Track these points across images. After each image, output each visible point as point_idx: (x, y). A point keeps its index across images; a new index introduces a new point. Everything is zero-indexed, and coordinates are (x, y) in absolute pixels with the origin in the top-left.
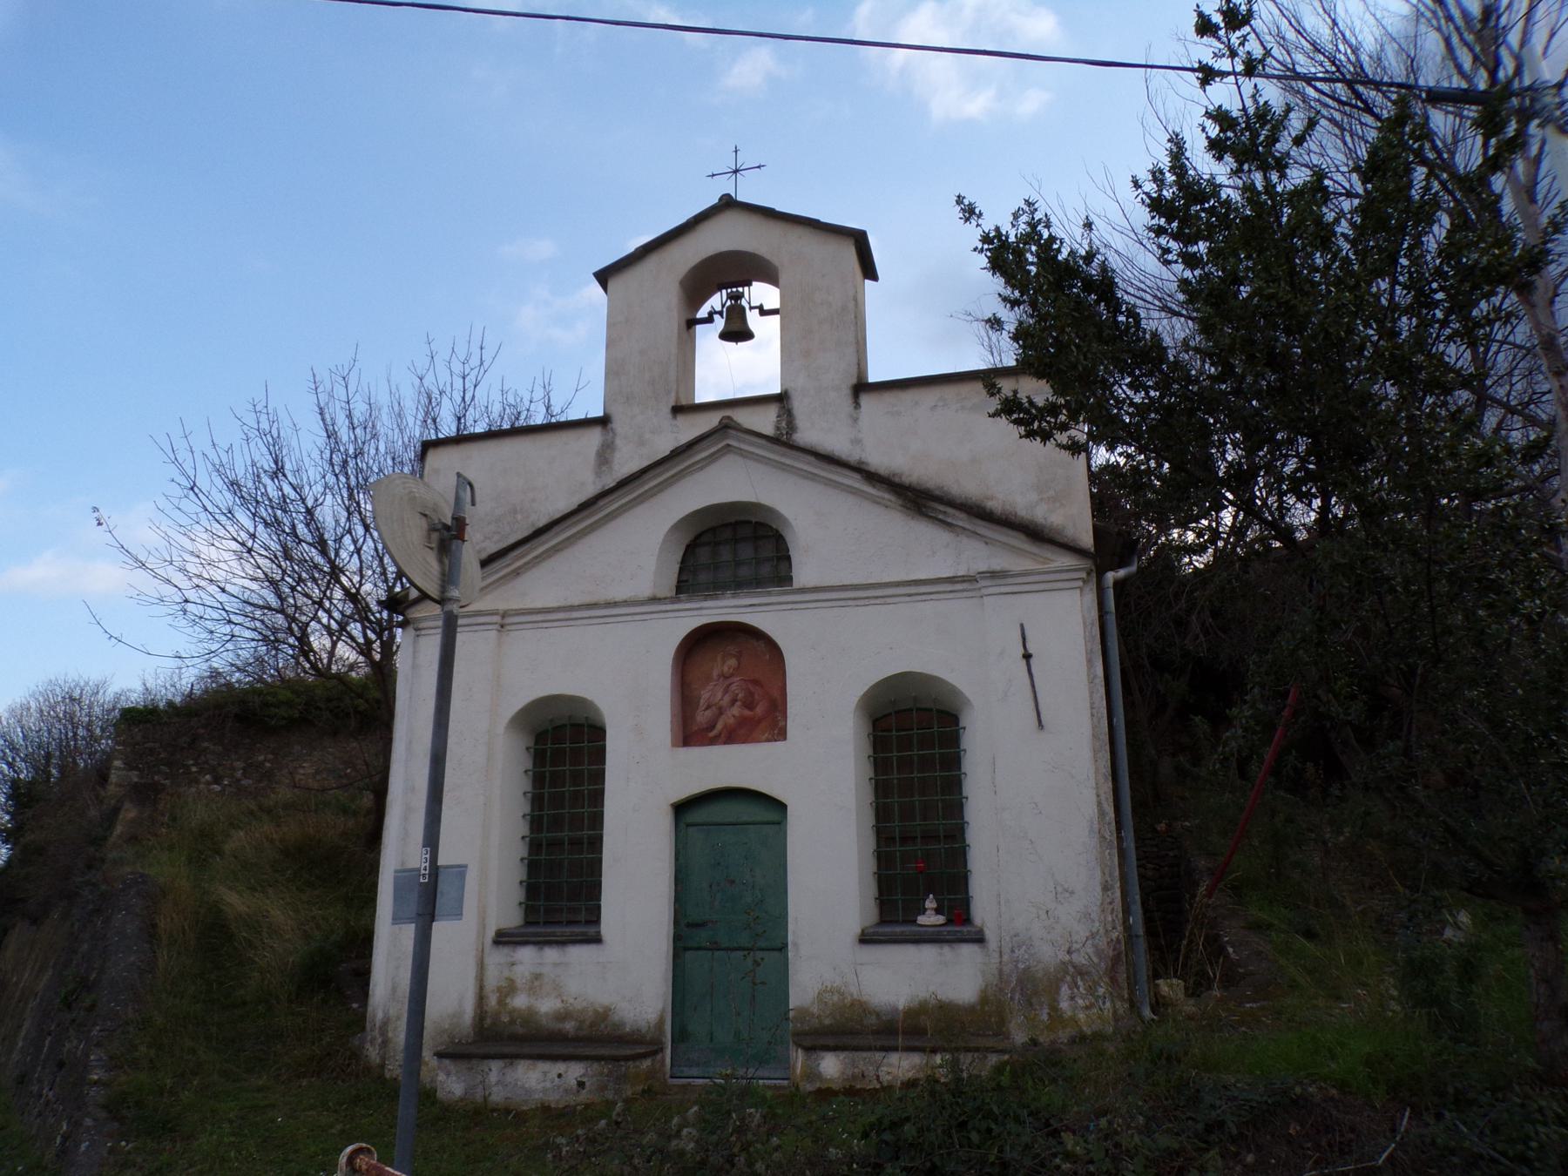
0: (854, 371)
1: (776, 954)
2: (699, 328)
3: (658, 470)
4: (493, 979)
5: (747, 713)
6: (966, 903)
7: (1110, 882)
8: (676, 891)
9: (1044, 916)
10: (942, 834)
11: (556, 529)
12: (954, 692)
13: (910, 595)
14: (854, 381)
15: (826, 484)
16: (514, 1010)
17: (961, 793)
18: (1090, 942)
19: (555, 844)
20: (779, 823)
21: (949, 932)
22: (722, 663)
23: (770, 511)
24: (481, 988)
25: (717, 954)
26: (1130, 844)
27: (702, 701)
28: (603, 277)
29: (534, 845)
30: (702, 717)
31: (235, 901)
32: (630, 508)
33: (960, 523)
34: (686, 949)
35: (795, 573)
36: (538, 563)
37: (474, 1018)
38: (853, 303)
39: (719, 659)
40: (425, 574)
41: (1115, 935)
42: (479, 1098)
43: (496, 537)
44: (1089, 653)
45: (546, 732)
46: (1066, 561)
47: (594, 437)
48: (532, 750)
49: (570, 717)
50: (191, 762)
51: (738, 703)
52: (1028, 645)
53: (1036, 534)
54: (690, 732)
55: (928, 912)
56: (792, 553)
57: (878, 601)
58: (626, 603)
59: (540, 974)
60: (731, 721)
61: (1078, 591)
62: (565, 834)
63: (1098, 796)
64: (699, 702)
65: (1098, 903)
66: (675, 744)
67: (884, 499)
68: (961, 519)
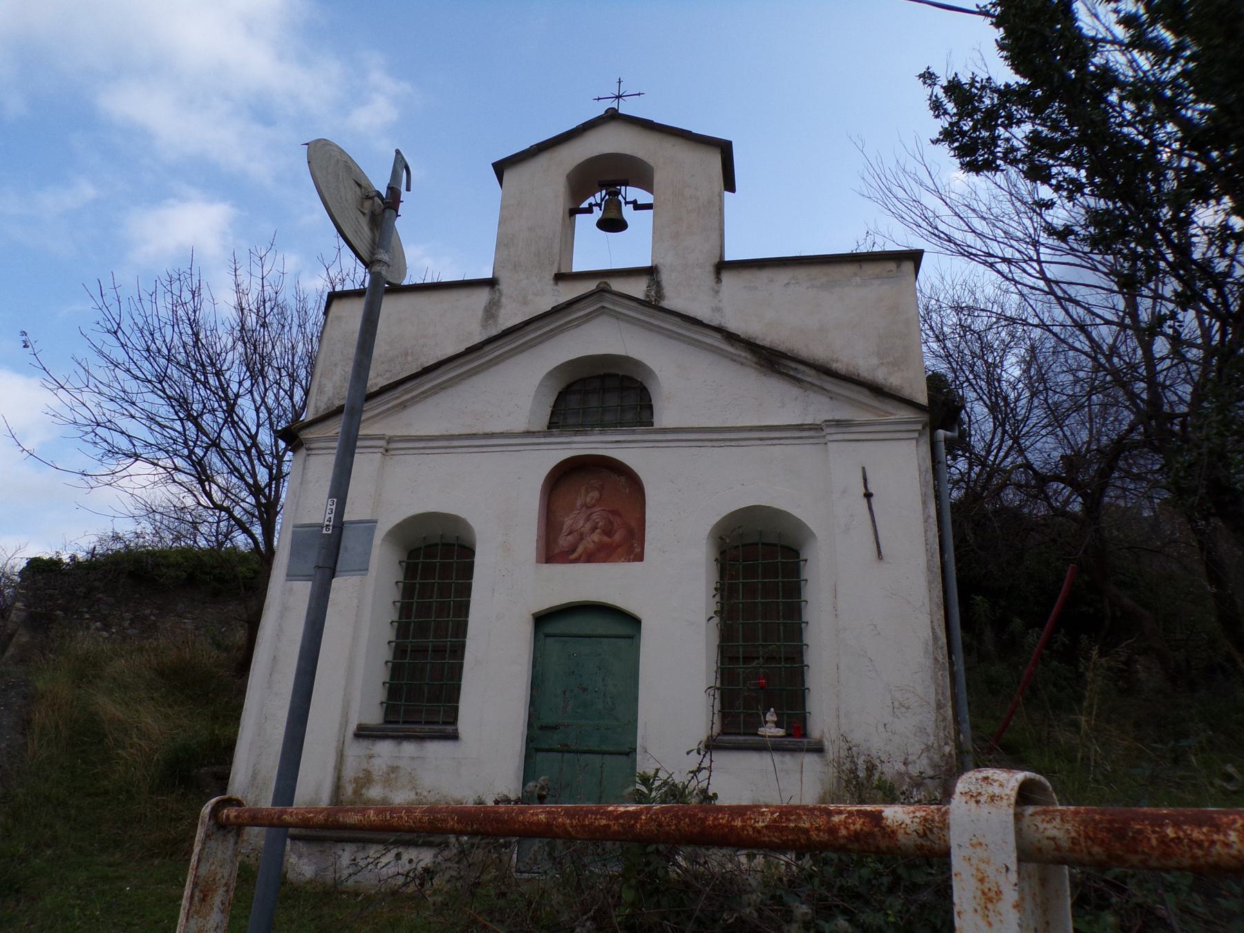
0: (718, 256)
1: (623, 758)
2: (579, 218)
4: (350, 772)
5: (606, 539)
7: (942, 701)
9: (881, 728)
11: (443, 369)
12: (799, 526)
13: (761, 439)
18: (925, 754)
19: (419, 651)
21: (789, 741)
22: (585, 494)
23: (637, 364)
25: (567, 756)
26: (960, 667)
28: (501, 168)
29: (399, 650)
30: (564, 541)
31: (108, 707)
32: (511, 356)
33: (809, 379)
34: (538, 750)
36: (426, 398)
38: (718, 198)
39: (583, 491)
40: (356, 232)
41: (947, 749)
42: (329, 876)
43: (388, 375)
44: (924, 495)
46: (905, 414)
47: (483, 295)
48: (404, 564)
49: (442, 536)
50: (85, 610)
51: (598, 531)
52: (869, 486)
53: (878, 391)
54: (551, 552)
55: (768, 725)
57: (733, 443)
58: (502, 435)
59: (397, 767)
60: (591, 546)
61: (915, 442)
63: (932, 622)
64: (562, 529)
65: (933, 719)
66: (538, 561)
67: (740, 356)
68: (810, 376)
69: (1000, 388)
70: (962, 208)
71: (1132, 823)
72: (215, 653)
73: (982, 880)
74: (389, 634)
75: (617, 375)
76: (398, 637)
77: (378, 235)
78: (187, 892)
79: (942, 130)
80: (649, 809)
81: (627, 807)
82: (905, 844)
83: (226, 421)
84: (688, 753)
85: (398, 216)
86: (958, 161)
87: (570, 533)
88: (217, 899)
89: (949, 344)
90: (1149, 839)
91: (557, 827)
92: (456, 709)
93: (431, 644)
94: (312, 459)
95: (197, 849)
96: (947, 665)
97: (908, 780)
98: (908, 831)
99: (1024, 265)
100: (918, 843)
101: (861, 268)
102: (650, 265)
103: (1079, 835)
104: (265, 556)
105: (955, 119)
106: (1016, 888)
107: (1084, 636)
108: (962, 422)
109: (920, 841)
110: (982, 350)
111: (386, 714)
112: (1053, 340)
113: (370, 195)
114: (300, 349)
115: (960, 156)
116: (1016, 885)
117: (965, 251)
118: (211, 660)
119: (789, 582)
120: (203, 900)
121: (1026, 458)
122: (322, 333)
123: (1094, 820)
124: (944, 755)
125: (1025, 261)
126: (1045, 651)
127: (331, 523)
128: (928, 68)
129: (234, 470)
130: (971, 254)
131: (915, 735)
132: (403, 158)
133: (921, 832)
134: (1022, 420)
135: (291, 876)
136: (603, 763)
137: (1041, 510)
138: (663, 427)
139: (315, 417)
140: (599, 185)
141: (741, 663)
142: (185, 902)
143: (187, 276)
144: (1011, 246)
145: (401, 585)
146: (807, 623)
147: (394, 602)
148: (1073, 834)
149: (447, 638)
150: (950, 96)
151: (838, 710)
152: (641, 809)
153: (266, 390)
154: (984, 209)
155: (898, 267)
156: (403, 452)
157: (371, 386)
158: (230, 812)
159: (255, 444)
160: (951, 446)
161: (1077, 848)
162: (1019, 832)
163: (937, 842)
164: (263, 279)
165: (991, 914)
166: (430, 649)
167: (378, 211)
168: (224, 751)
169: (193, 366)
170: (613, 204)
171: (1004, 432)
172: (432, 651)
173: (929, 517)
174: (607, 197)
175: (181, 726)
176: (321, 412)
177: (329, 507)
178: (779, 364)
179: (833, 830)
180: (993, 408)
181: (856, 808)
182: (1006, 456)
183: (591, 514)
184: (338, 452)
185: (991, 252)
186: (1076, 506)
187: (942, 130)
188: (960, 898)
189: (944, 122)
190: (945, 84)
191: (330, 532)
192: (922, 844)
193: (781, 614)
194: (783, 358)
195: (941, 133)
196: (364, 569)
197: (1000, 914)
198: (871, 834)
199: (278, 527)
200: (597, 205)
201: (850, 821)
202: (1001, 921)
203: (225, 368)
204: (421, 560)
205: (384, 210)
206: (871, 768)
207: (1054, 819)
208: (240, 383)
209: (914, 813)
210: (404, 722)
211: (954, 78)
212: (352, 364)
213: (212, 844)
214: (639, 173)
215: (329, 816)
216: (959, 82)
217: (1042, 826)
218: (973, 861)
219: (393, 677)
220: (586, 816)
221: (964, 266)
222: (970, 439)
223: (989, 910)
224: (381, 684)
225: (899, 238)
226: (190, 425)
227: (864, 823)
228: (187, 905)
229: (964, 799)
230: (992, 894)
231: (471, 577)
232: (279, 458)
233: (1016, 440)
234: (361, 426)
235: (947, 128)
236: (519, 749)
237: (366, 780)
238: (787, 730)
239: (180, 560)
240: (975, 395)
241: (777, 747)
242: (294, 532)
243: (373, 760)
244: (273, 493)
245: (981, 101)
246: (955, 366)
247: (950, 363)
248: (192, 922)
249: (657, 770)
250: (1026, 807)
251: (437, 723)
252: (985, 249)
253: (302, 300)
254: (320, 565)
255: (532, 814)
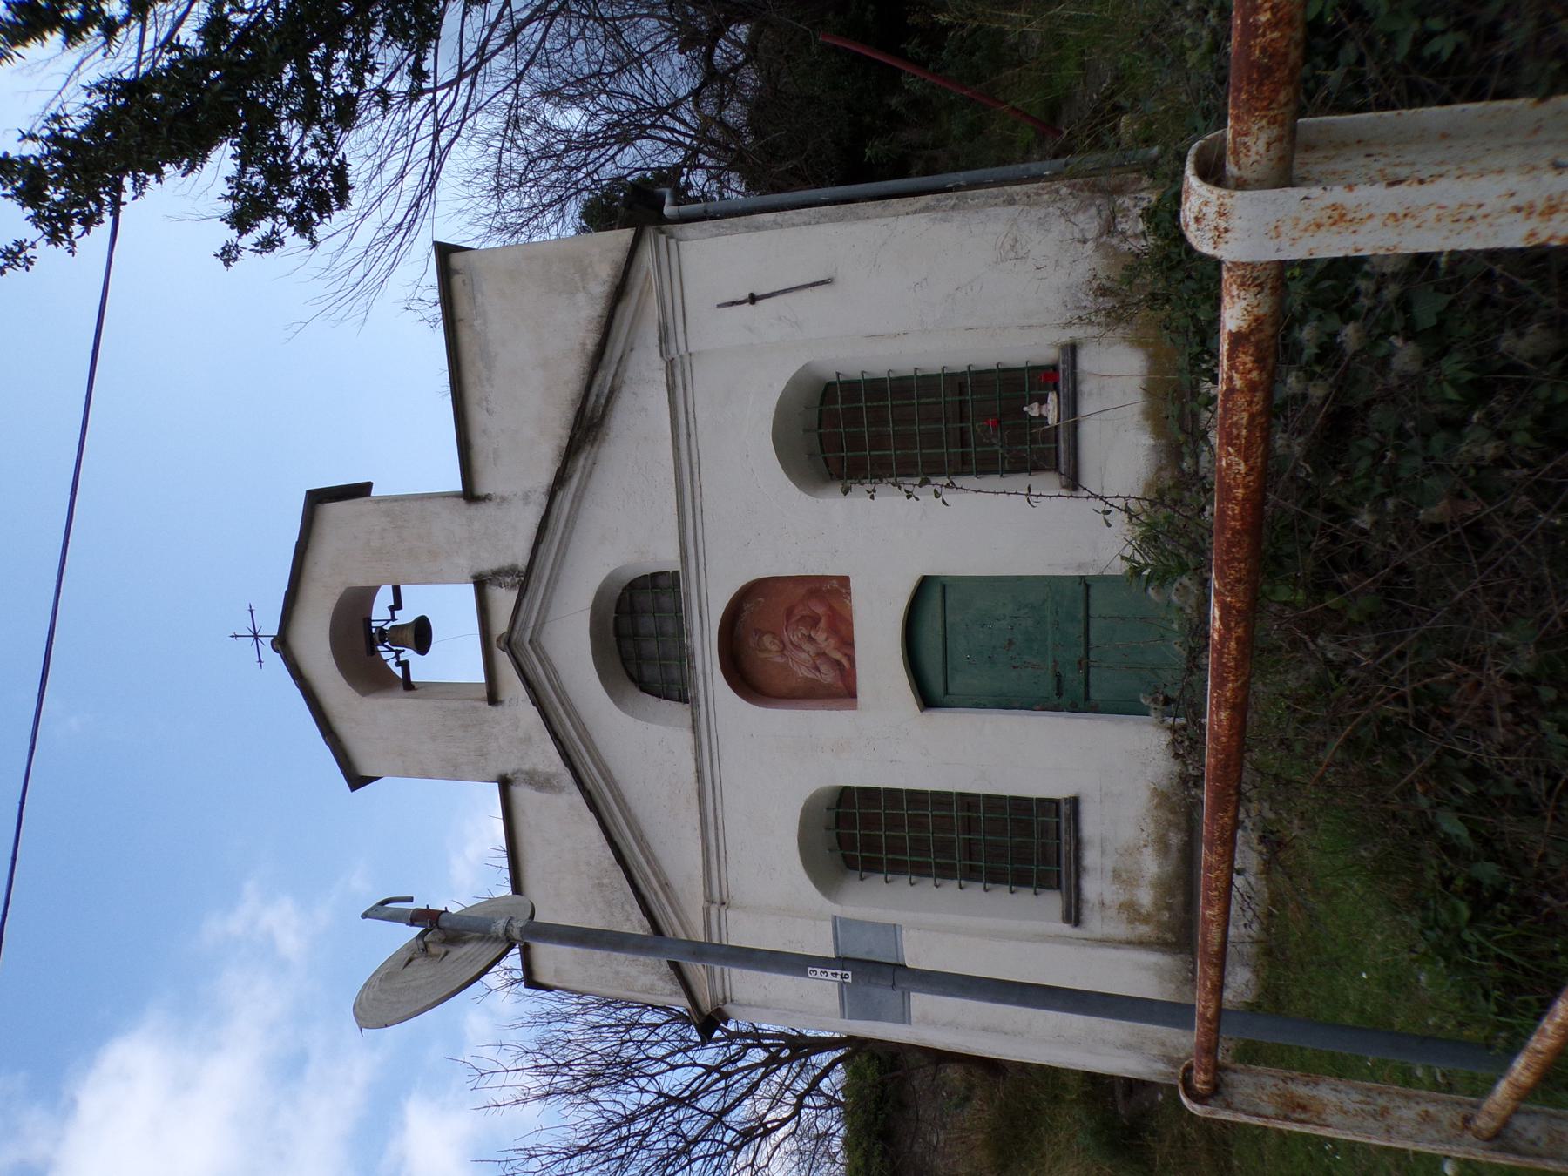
0: (455, 499)
1: (1093, 592)
3: (553, 717)
4: (1121, 930)
5: (823, 624)
6: (1034, 370)
8: (1021, 708)
9: (1041, 274)
10: (957, 398)
11: (617, 838)
12: (795, 384)
13: (689, 435)
14: (462, 501)
15: (571, 531)
16: (1155, 904)
17: (910, 378)
19: (970, 850)
20: (944, 587)
22: (768, 653)
24: (1129, 943)
26: (961, 177)
27: (810, 676)
28: (357, 780)
29: (971, 874)
30: (828, 676)
32: (596, 750)
33: (610, 378)
34: (1087, 698)
35: (670, 569)
37: (1164, 952)
39: (762, 655)
42: (1248, 949)
43: (628, 907)
44: (750, 228)
45: (844, 857)
46: (647, 256)
47: (521, 793)
48: (864, 874)
49: (827, 829)
53: (619, 291)
55: (1044, 413)
56: (648, 572)
57: (696, 471)
60: (832, 642)
62: (958, 837)
63: (907, 214)
66: (854, 707)
67: (584, 467)
68: (605, 378)
69: (598, 132)
70: (371, 194)
71: (1252, 59)
72: (976, 1103)
73: (1319, 226)
74: (951, 888)
75: (616, 619)
76: (953, 878)
77: (473, 934)
78: (1296, 1128)
79: (297, 235)
80: (1218, 593)
81: (1214, 617)
82: (1270, 307)
83: (689, 1106)
84: (1109, 525)
85: (446, 911)
86: (336, 213)
87: (817, 669)
88: (1301, 1090)
89: (545, 200)
90: (1272, 40)
91: (1236, 697)
92: (1041, 801)
93: (961, 837)
94: (737, 996)
95: (1244, 1119)
96: (959, 193)
97: (1105, 237)
98: (1256, 303)
99: (441, 111)
100: (1269, 291)
101: (462, 320)
102: (472, 585)
103: (1265, 116)
104: (855, 1047)
105: (281, 219)
106: (1329, 188)
107: (909, 20)
108: (643, 179)
109: (1267, 291)
110: (549, 157)
111: (1050, 888)
112: (533, 68)
113: (423, 946)
114: (594, 1018)
115: (330, 210)
116: (1325, 189)
117: (428, 186)
118: (985, 1108)
119: (865, 393)
120: (1304, 1108)
121: (685, 98)
122: (573, 992)
123: (1248, 100)
124: (1071, 194)
125: (435, 111)
126: (931, 67)
127: (839, 972)
128: (216, 255)
129: (750, 1092)
130: (431, 179)
131: (1048, 231)
132: (372, 909)
133: (1256, 290)
134: (636, 103)
135: (1249, 997)
136: (1100, 616)
137: (750, 78)
138: (679, 559)
139: (684, 995)
140: (373, 654)
141: (968, 450)
142: (1308, 1129)
143: (508, 1166)
144: (418, 127)
145: (889, 877)
146: (916, 369)
147: (912, 884)
148: (1264, 122)
149: (952, 817)
150: (252, 226)
151: (1022, 327)
152: (1218, 602)
153: (648, 1058)
154: (369, 164)
155: (457, 272)
156: (724, 883)
157: (642, 927)
158: (1200, 1080)
159: (717, 1069)
160: (681, 195)
161: (1280, 118)
162: (1260, 184)
163: (1268, 272)
164: (508, 1071)
165: (1358, 215)
166: (967, 837)
167: (440, 936)
168: (1097, 1085)
169: (621, 1152)
170: (396, 636)
171: (653, 125)
172: (969, 834)
173: (775, 222)
174: (387, 644)
175: (1068, 1140)
176: (679, 988)
177: (819, 976)
178: (592, 418)
179: (1252, 387)
180: (625, 140)
181: (1225, 361)
182: (683, 122)
183: (792, 643)
184: (726, 965)
185: (428, 154)
186: (742, 31)
187: (297, 235)
188: (1339, 249)
189: (288, 233)
190: (235, 232)
191: (850, 973)
192: (1271, 288)
193: (907, 402)
194: (583, 415)
195: (302, 236)
196: (894, 929)
197: (1359, 205)
198: (1257, 345)
199: (828, 1035)
200: (397, 657)
201: (1241, 367)
202: (1368, 204)
203: (621, 1111)
204: (858, 854)
205: (440, 928)
206: (1103, 291)
207: (1245, 143)
208: (642, 1091)
209: (1233, 297)
210: (1058, 864)
211: (227, 222)
212: (615, 954)
213: (1237, 1100)
214: (355, 605)
215: (1211, 963)
216: (232, 215)
217: (1254, 157)
218: (1296, 235)
219: (1003, 882)
220: (1224, 665)
221: (445, 185)
222: (664, 168)
223: (1354, 218)
224: (1014, 895)
225: (420, 270)
226: (697, 1149)
227: (1244, 353)
228: (1311, 1126)
229: (1222, 245)
230: (1336, 215)
231: (877, 790)
232: (731, 1037)
233: (662, 111)
234: (694, 939)
235: (295, 229)
236: (1086, 721)
237: (1130, 910)
238: (1049, 390)
239: (860, 1151)
240: (608, 166)
241: (1071, 404)
242: (851, 1018)
243: (1107, 902)
244: (776, 1042)
245: (255, 188)
246: (572, 191)
247: (569, 197)
248: (1331, 1120)
249: (1123, 558)
250: (1229, 174)
251: (1058, 824)
252: (424, 163)
253: (535, 1019)
254: (890, 984)
255: (1220, 726)
